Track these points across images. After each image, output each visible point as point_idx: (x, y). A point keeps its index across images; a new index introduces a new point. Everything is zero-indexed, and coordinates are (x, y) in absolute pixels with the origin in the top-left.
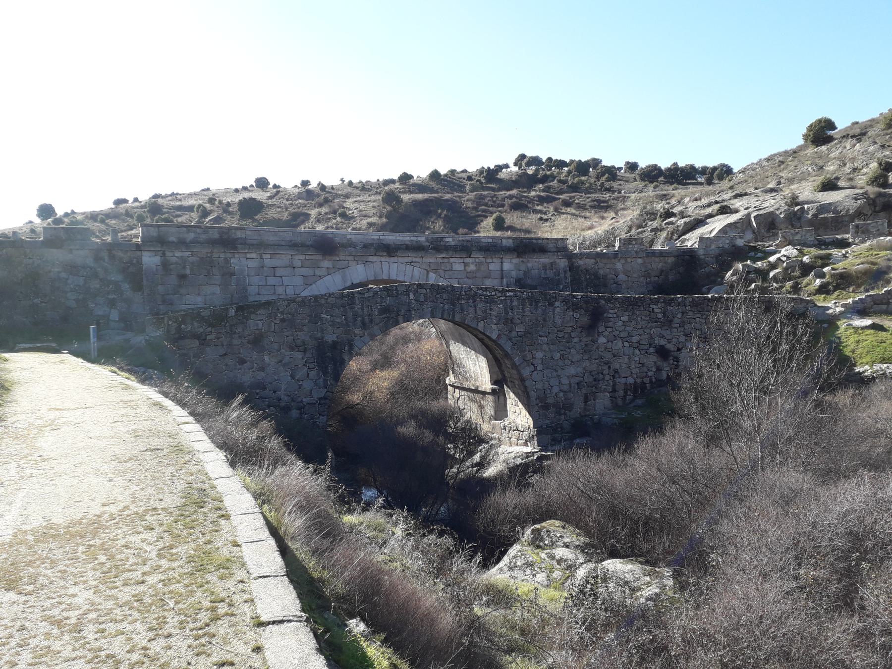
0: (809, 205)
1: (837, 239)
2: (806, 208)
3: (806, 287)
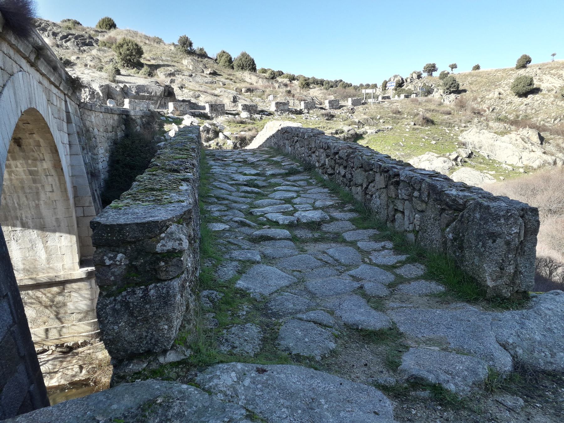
0: (130, 84)
1: (201, 113)
2: (128, 86)
3: (223, 145)
